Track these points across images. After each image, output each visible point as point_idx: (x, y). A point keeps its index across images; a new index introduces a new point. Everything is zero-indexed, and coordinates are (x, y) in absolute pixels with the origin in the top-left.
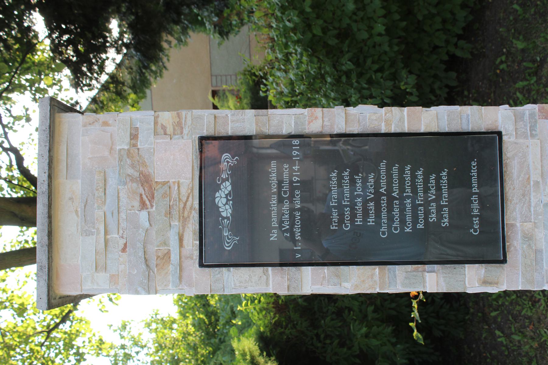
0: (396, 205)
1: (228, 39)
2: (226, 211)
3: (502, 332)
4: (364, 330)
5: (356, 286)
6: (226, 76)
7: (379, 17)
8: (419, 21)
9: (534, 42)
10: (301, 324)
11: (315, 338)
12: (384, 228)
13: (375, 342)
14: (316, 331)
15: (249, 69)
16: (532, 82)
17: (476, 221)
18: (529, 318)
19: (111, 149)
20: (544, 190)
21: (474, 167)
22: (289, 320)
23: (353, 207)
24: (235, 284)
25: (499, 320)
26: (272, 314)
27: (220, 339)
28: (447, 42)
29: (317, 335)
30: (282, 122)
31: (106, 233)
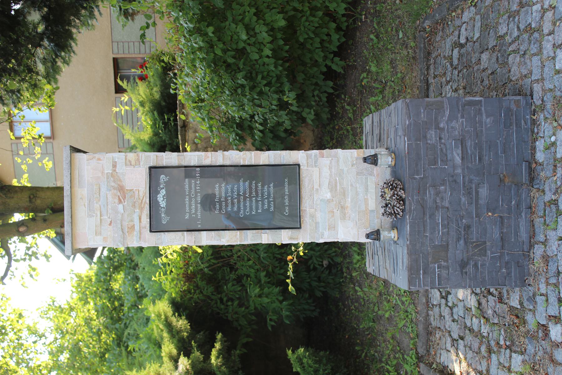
1: (133, 20)
2: (163, 204)
3: (361, 289)
4: (257, 290)
5: (228, 241)
10: (207, 289)
11: (219, 301)
12: (242, 212)
13: (266, 300)
17: (287, 208)
19: (103, 172)
23: (226, 200)
26: (182, 282)
27: (125, 324)
28: (325, 58)
29: (221, 300)
31: (101, 216)
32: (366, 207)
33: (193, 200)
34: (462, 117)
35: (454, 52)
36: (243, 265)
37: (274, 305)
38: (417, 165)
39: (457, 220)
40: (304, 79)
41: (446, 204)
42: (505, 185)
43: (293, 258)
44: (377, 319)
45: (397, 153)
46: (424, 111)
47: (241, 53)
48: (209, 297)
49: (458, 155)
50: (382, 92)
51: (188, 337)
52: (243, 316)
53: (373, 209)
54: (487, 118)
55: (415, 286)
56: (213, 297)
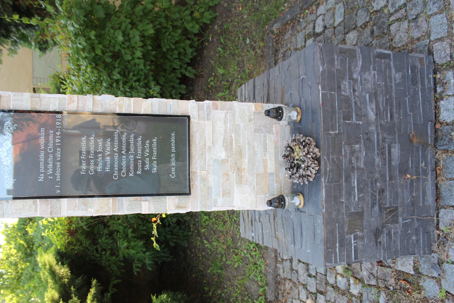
0: (124, 159)
3: (208, 241)
4: (126, 244)
5: (97, 211)
6: (44, 79)
7: (139, 47)
8: (164, 52)
9: (228, 70)
10: (86, 242)
11: (95, 251)
13: (132, 252)
14: (95, 247)
15: (57, 74)
16: (227, 93)
18: (222, 232)
20: (214, 152)
21: (173, 136)
22: (78, 240)
24: (12, 211)
25: (206, 234)
26: (66, 237)
28: (181, 67)
29: (97, 250)
30: (50, 102)
32: (264, 170)
33: (51, 157)
34: (374, 70)
35: (307, 43)
36: (114, 223)
37: (139, 255)
38: (332, 119)
39: (372, 183)
40: (164, 82)
41: (362, 165)
42: (413, 145)
43: (157, 219)
44: (225, 267)
45: (304, 106)
46: (338, 58)
47: (116, 56)
48: (87, 248)
49: (373, 110)
50: (229, 88)
51: (68, 282)
52: (114, 263)
53: (272, 172)
54: (396, 73)
55: (331, 262)
56: (90, 248)
